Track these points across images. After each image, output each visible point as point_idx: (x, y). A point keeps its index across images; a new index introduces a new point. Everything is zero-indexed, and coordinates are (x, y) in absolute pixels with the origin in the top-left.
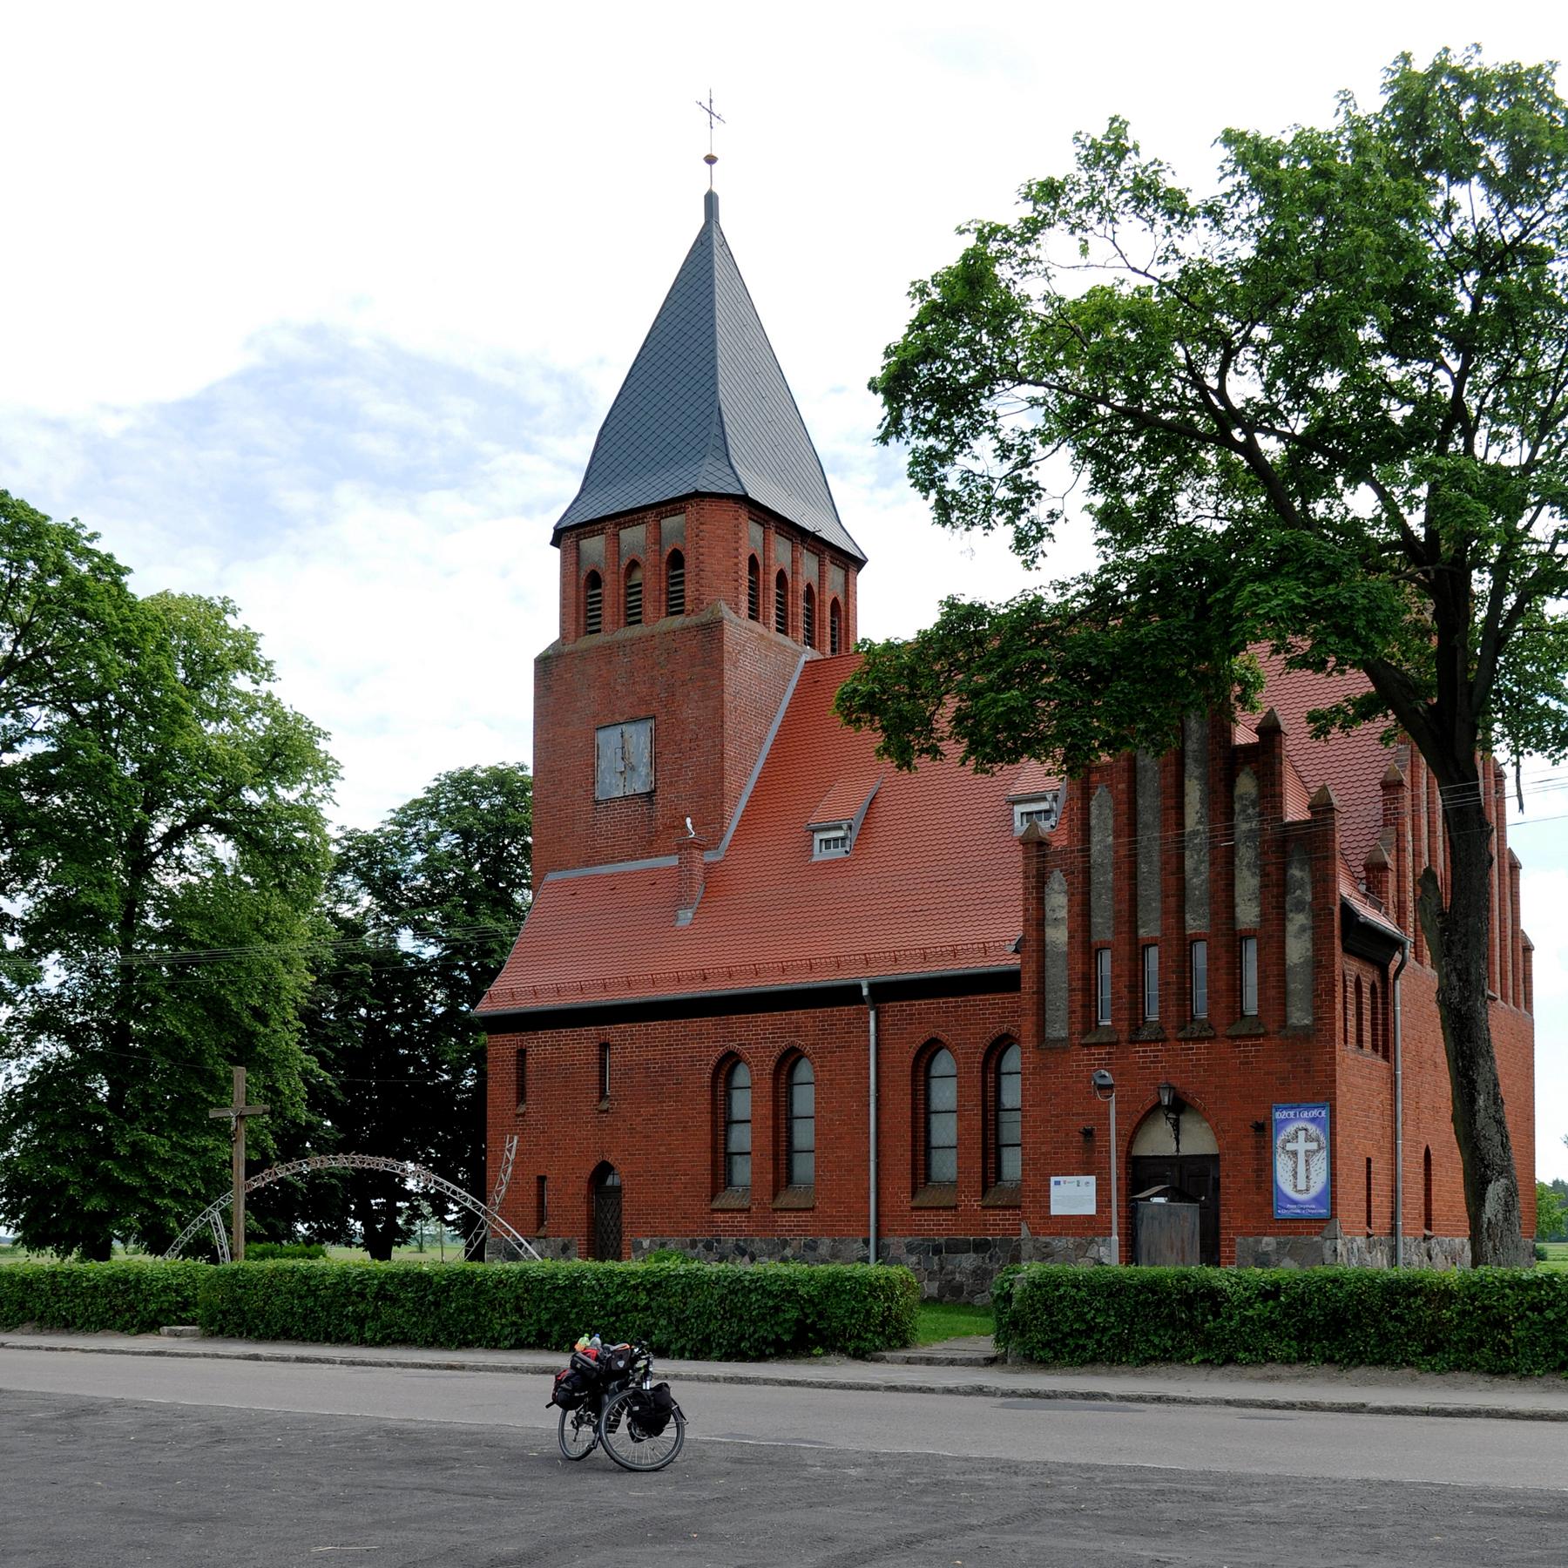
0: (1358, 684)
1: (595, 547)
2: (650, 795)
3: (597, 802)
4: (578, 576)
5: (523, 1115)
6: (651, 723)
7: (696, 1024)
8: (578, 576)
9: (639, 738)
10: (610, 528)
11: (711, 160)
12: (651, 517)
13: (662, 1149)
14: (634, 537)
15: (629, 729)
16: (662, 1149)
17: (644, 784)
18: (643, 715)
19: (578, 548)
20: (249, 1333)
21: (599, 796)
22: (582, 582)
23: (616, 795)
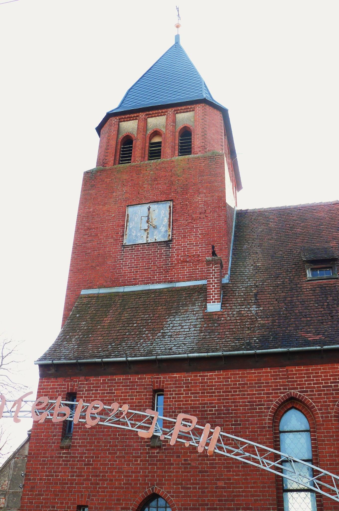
0: (18, 418)
1: (130, 126)
2: (167, 243)
3: (124, 246)
4: (117, 137)
5: (68, 448)
6: (171, 204)
7: (253, 374)
8: (117, 137)
9: (161, 212)
10: (142, 115)
11: (178, 27)
12: (170, 111)
13: (221, 484)
14: (156, 122)
15: (154, 207)
16: (221, 484)
17: (164, 236)
18: (163, 199)
19: (119, 125)
20: (85, 199)
21: (126, 241)
22: (120, 140)
23: (140, 242)
